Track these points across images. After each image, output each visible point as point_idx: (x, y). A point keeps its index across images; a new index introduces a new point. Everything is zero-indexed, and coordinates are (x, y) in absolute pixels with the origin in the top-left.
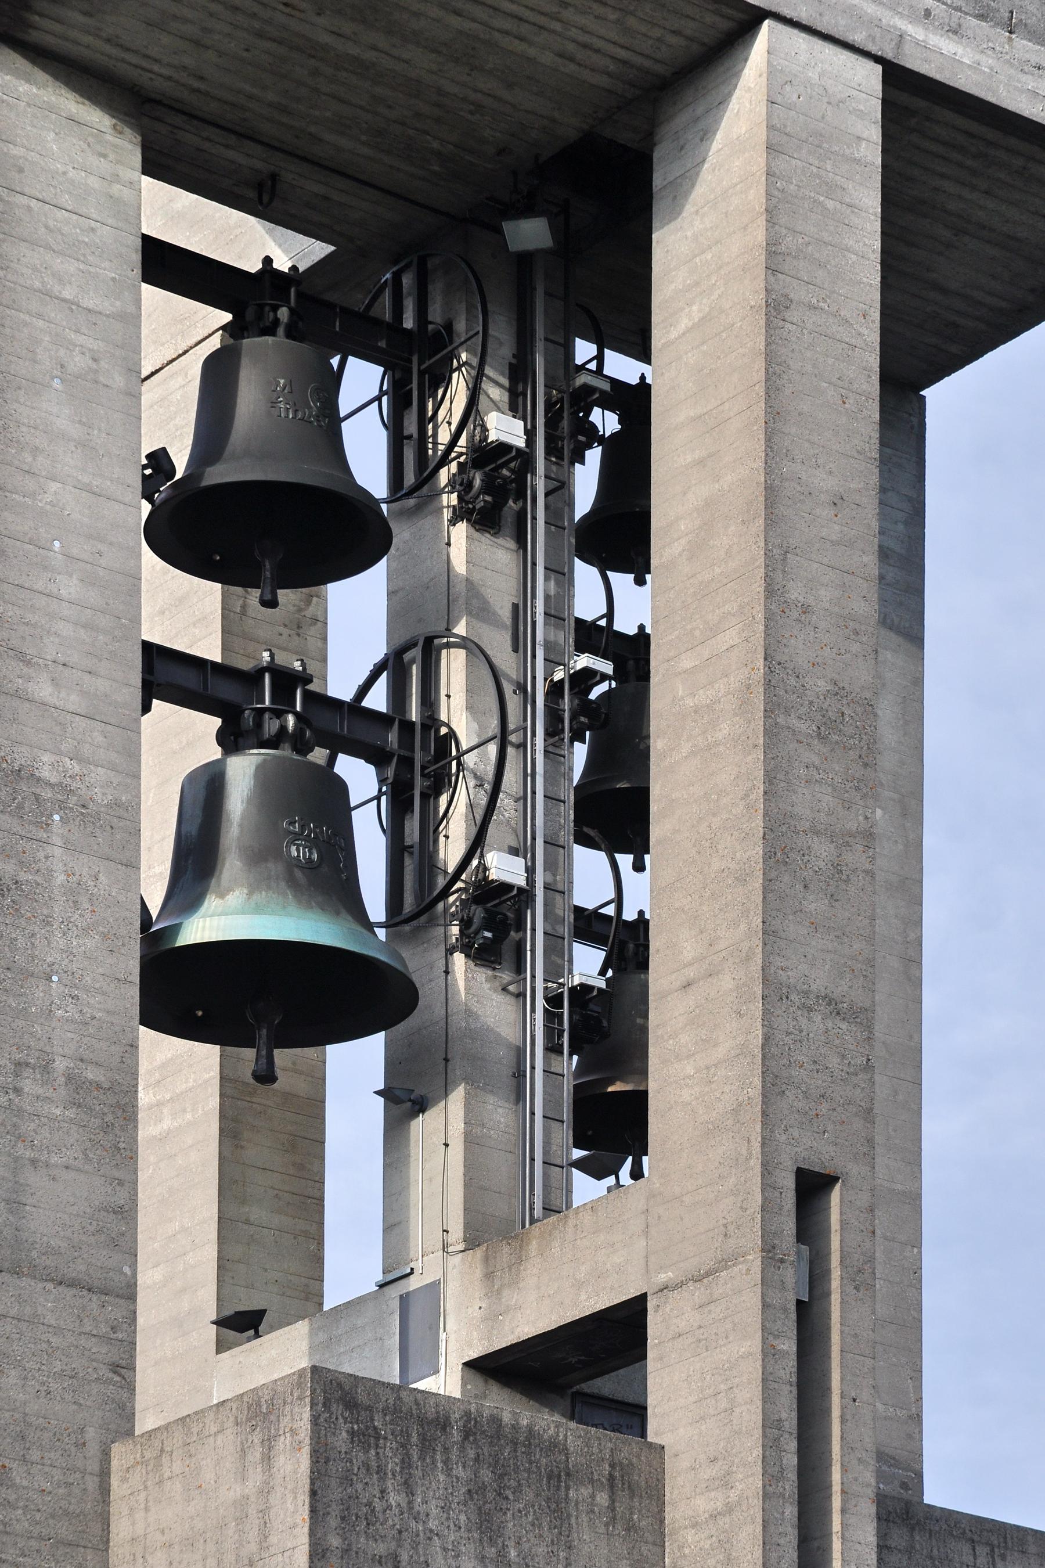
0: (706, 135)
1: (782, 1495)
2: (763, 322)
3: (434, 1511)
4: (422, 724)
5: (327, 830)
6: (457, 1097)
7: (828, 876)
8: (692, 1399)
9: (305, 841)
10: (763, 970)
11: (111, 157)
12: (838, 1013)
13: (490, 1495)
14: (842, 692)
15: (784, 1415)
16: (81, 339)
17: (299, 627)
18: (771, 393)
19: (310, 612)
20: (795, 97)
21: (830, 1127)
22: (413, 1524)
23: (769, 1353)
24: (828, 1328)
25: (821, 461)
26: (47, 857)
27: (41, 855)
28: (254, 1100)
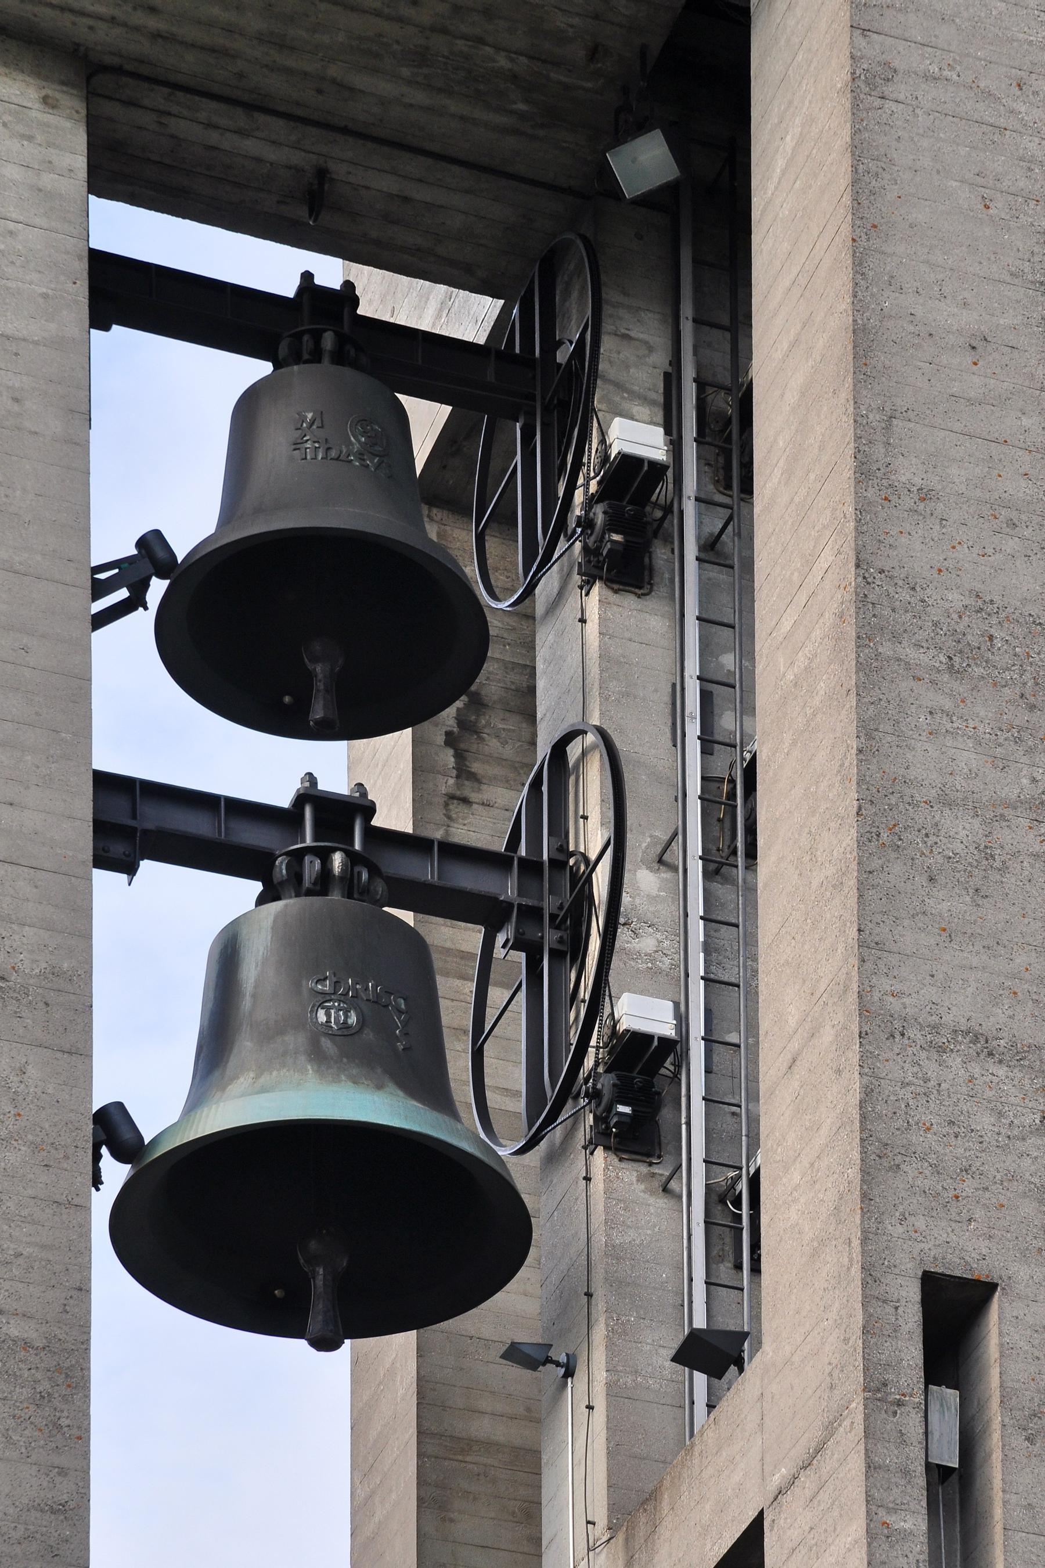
2: (848, 105)
5: (375, 987)
7: (970, 864)
9: (340, 1001)
10: (860, 997)
11: (39, 138)
12: (991, 1054)
14: (990, 608)
18: (863, 199)
21: (979, 1213)
25: (946, 290)
28: (468, 1459)
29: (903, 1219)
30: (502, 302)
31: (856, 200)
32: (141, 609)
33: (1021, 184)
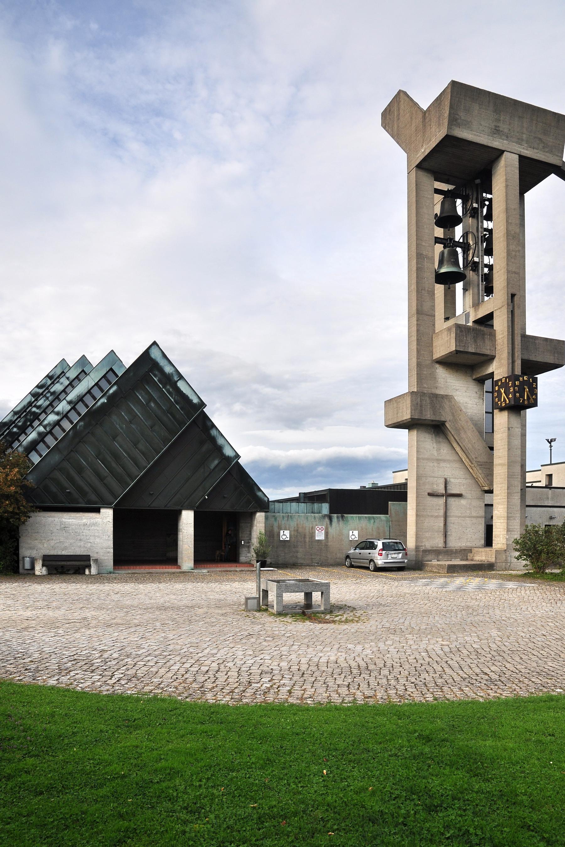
6: (471, 288)
23: (508, 317)
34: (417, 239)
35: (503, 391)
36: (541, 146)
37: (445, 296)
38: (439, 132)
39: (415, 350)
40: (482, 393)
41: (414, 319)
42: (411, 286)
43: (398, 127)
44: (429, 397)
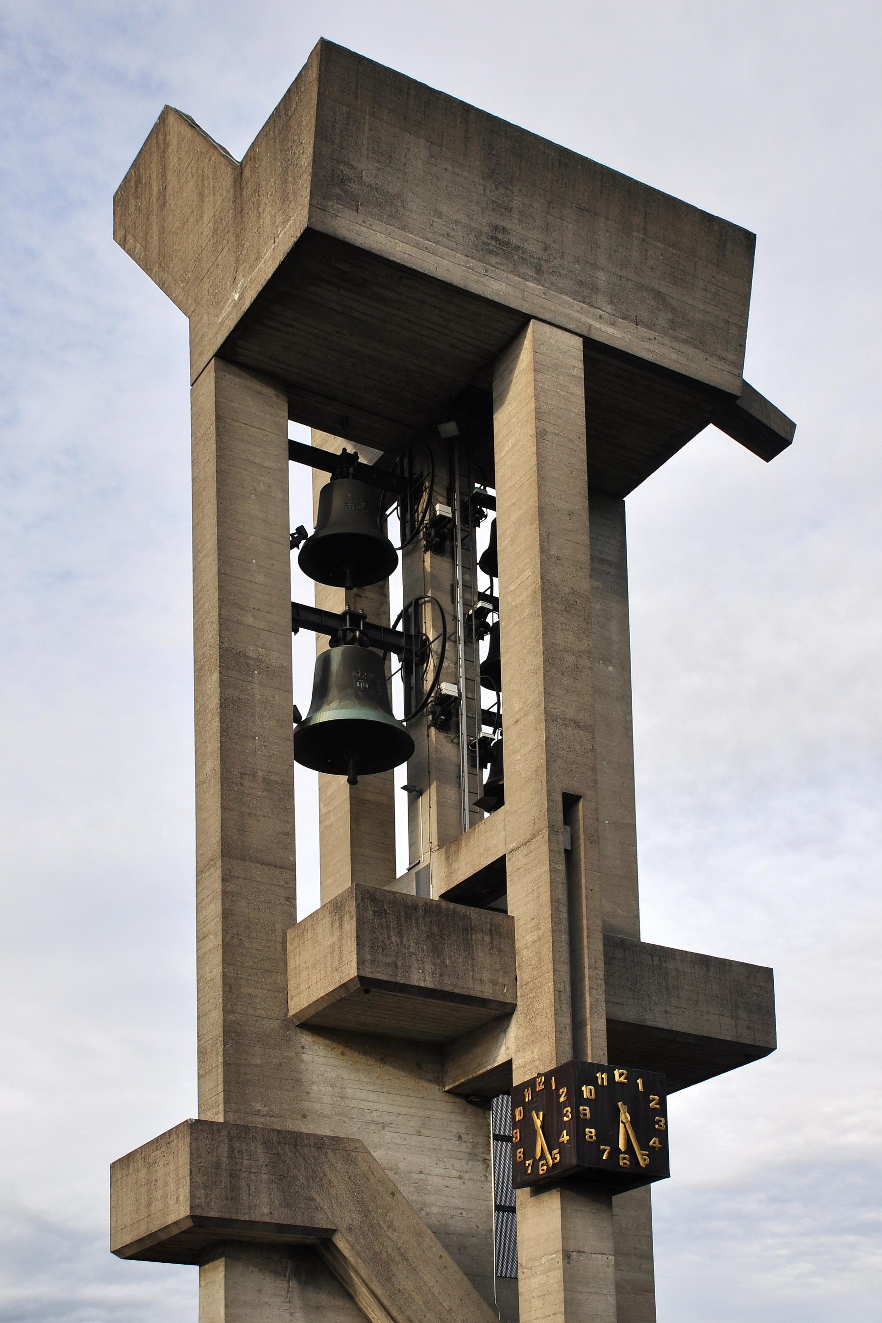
0: (512, 371)
1: (561, 930)
2: (535, 441)
3: (412, 944)
4: (415, 635)
6: (434, 787)
8: (524, 895)
13: (437, 938)
15: (560, 897)
16: (263, 479)
17: (378, 615)
19: (383, 609)
20: (545, 351)
22: (403, 950)
23: (553, 870)
24: (580, 860)
26: (252, 688)
27: (250, 687)
29: (557, 777)
30: (383, 453)
31: (538, 470)
32: (296, 548)
33: (581, 467)
34: (221, 600)
35: (538, 1123)
36: (663, 319)
37: (352, 819)
38: (285, 222)
39: (219, 981)
40: (481, 1140)
41: (215, 875)
42: (204, 763)
43: (162, 231)
44: (267, 1143)
